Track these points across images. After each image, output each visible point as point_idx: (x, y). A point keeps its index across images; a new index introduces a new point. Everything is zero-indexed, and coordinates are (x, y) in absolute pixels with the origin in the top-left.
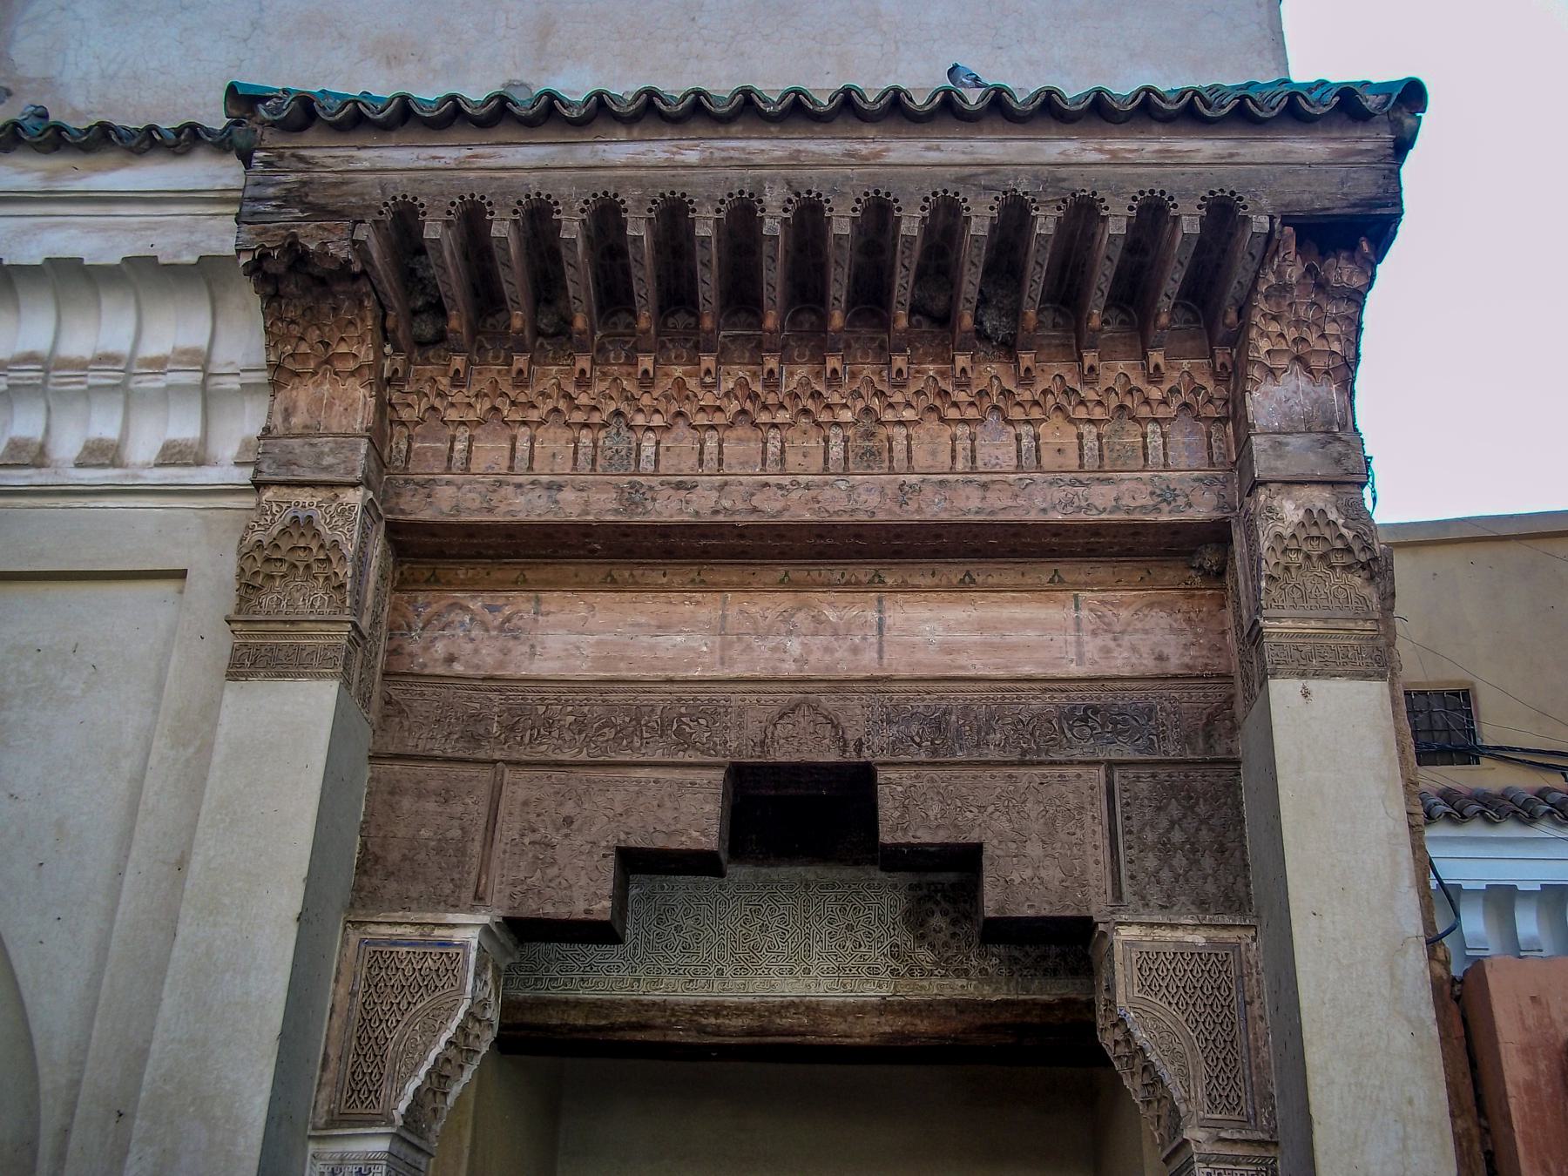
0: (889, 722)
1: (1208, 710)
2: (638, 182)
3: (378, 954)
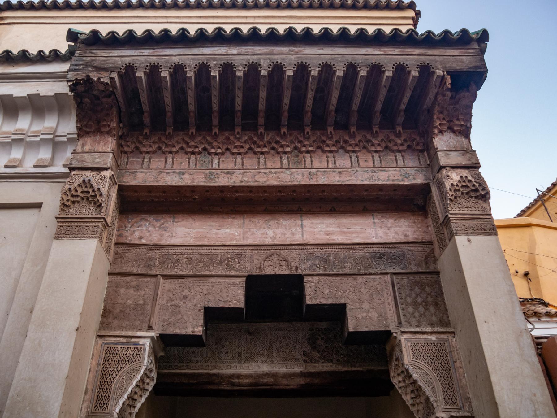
0: (308, 260)
1: (425, 254)
2: (215, 59)
3: (109, 348)
